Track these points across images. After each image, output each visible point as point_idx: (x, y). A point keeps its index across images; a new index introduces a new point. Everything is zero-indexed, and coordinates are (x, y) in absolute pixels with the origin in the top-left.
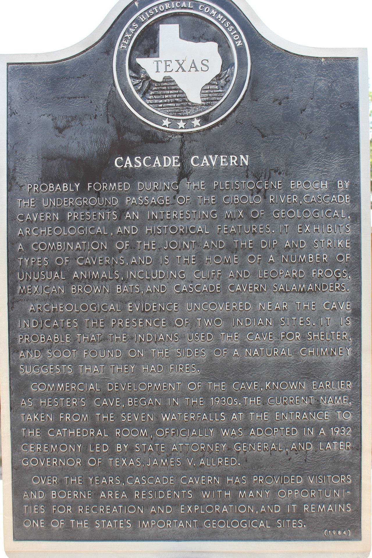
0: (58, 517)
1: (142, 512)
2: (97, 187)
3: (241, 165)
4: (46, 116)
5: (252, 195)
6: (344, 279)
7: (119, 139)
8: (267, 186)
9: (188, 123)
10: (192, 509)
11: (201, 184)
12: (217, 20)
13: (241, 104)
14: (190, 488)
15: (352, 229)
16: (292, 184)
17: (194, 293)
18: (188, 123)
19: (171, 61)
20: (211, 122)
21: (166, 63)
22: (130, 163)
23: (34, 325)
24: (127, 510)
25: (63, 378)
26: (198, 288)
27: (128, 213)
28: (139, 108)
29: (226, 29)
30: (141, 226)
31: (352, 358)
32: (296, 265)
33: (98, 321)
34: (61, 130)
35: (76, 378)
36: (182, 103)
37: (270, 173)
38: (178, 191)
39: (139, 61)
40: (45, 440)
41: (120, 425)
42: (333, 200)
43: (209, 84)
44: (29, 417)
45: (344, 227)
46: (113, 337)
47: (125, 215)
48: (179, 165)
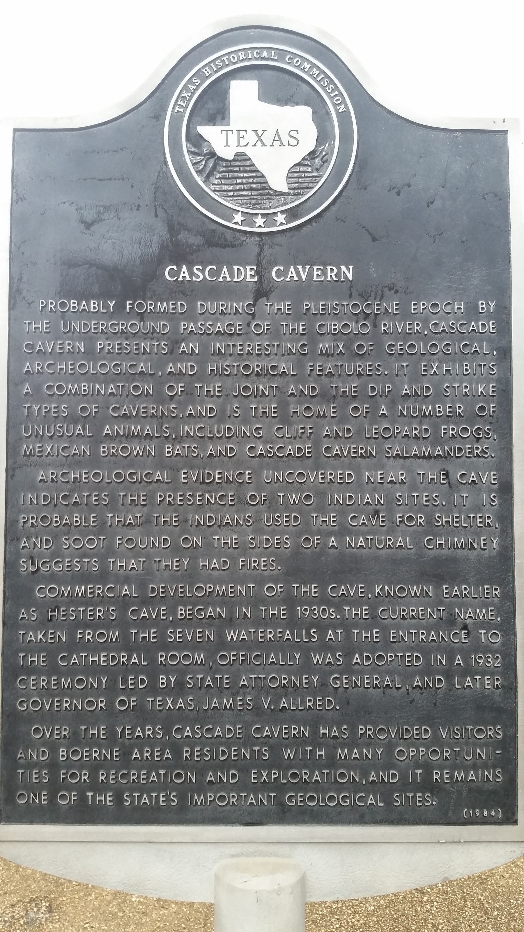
0: (69, 788)
1: (194, 781)
2: (140, 305)
3: (342, 279)
4: (67, 204)
5: (357, 322)
6: (487, 440)
7: (171, 241)
8: (378, 309)
9: (269, 218)
10: (269, 775)
11: (285, 306)
12: (311, 76)
13: (344, 194)
14: (265, 744)
15: (498, 370)
16: (413, 307)
17: (275, 457)
18: (269, 218)
19: (246, 131)
20: (301, 218)
21: (238, 134)
22: (187, 275)
23: (44, 501)
24: (171, 778)
25: (84, 578)
26: (281, 450)
27: (183, 344)
28: (201, 196)
29: (324, 88)
30: (202, 364)
31: (500, 553)
32: (418, 419)
33: (138, 496)
34: (88, 225)
35: (103, 576)
36: (261, 192)
37: (383, 291)
38: (253, 315)
39: (202, 130)
40: (53, 669)
41: (165, 646)
42: (471, 328)
43: (298, 164)
44: (31, 636)
45: (487, 367)
46: (159, 518)
47: (179, 348)
48: (255, 279)
